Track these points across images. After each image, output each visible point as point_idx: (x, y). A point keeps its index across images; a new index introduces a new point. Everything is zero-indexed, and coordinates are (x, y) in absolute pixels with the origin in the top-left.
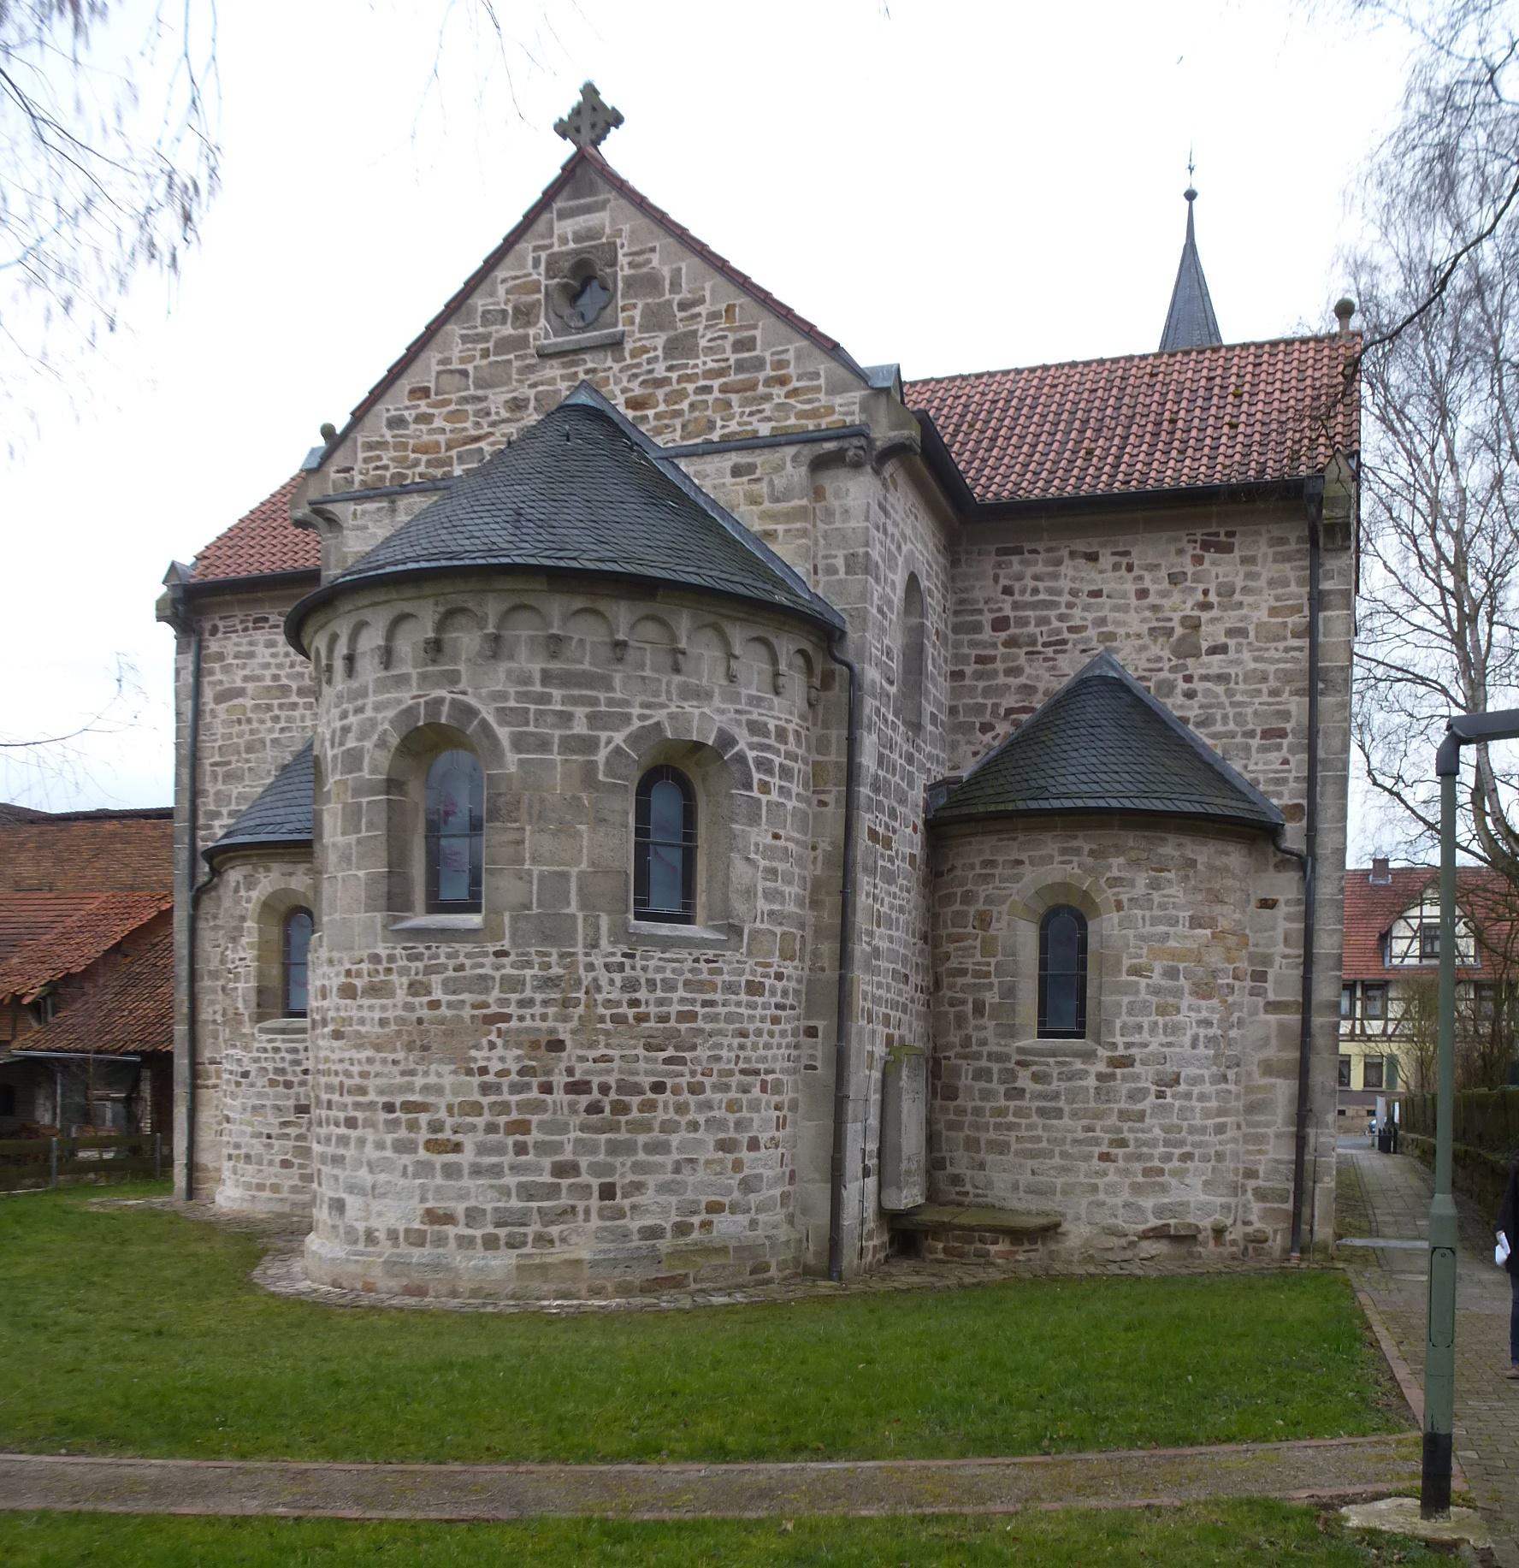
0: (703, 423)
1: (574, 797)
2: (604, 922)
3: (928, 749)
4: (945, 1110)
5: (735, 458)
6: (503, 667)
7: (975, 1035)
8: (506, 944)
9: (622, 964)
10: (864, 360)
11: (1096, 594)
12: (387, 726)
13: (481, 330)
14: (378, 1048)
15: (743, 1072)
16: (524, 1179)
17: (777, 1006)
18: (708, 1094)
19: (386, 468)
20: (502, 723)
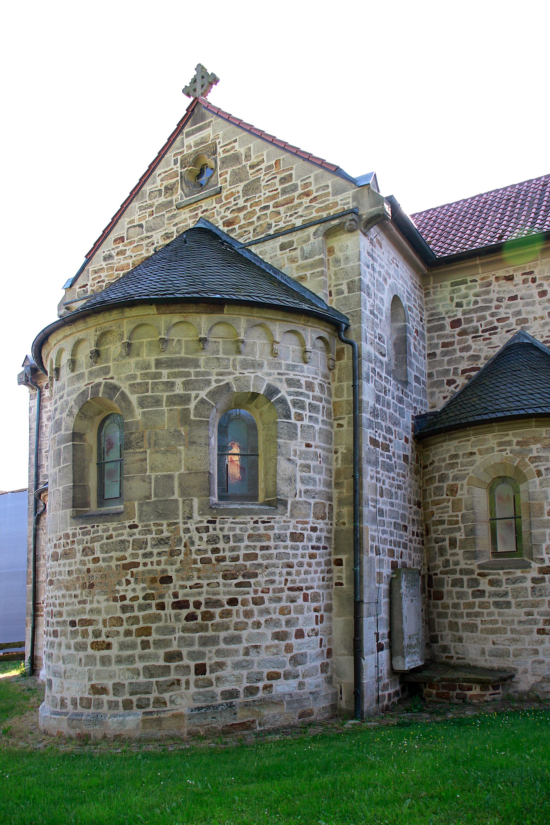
0: (265, 226)
1: (176, 431)
2: (196, 502)
3: (414, 396)
4: (436, 606)
5: (282, 240)
6: (133, 361)
7: (451, 559)
8: (136, 521)
9: (208, 527)
10: (354, 174)
11: (514, 298)
12: (73, 403)
13: (149, 202)
14: (68, 588)
15: (290, 589)
16: (147, 664)
17: (313, 548)
18: (267, 604)
19: (103, 281)
20: (133, 393)
